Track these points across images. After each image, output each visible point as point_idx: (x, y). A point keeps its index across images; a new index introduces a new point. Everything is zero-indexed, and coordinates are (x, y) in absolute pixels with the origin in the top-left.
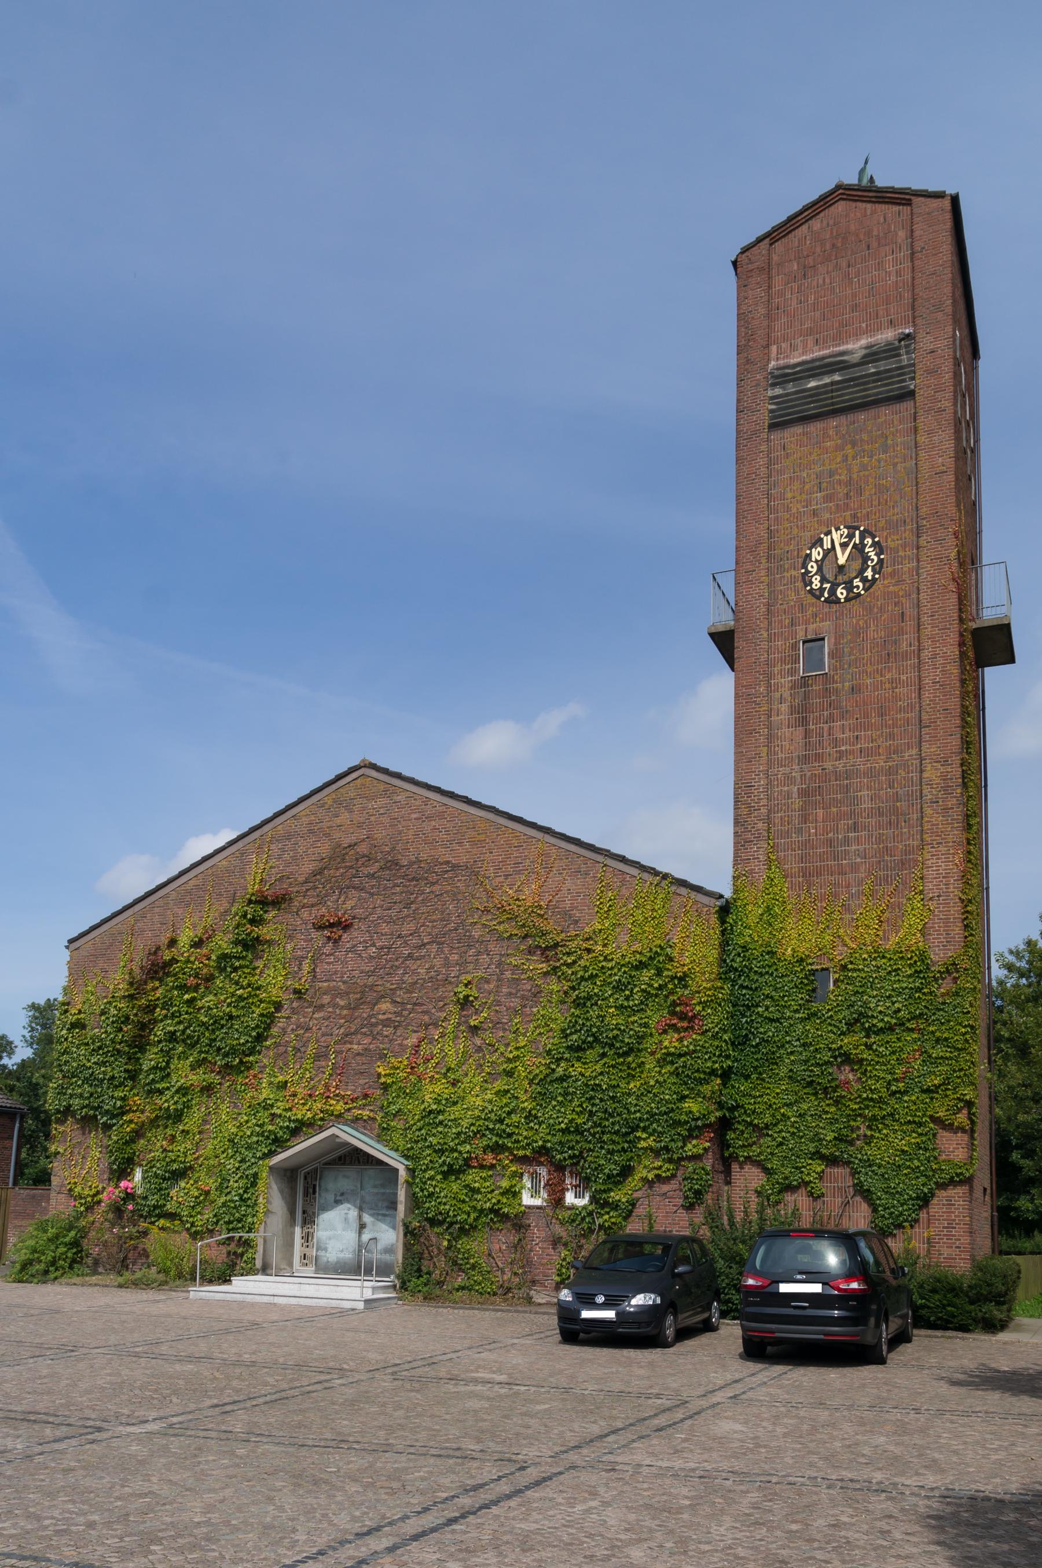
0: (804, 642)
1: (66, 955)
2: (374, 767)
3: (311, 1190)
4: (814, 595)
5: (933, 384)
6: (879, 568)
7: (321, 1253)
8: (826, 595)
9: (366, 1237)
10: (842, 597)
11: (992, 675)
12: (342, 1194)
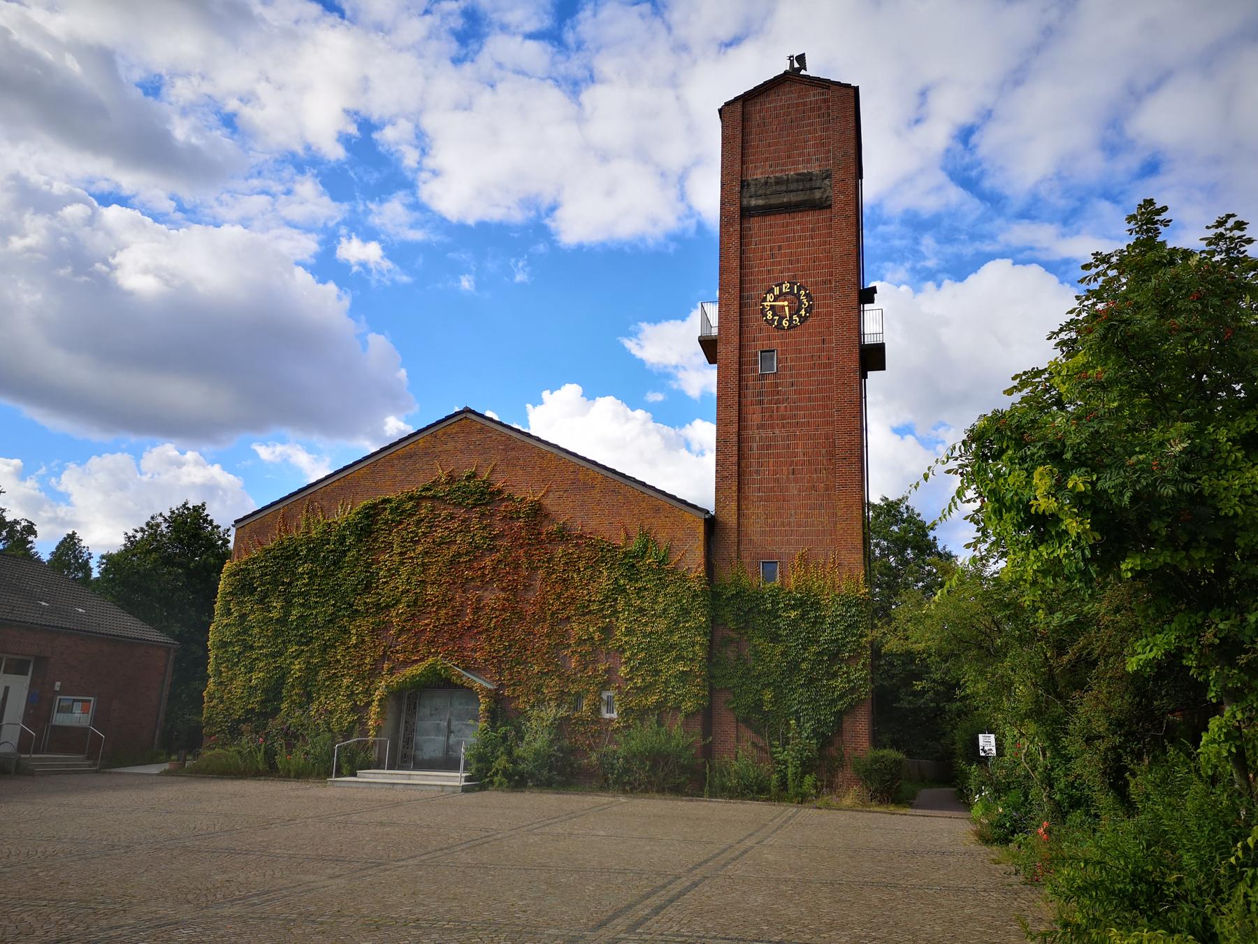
2: (473, 412)
7: (418, 753)
9: (453, 739)
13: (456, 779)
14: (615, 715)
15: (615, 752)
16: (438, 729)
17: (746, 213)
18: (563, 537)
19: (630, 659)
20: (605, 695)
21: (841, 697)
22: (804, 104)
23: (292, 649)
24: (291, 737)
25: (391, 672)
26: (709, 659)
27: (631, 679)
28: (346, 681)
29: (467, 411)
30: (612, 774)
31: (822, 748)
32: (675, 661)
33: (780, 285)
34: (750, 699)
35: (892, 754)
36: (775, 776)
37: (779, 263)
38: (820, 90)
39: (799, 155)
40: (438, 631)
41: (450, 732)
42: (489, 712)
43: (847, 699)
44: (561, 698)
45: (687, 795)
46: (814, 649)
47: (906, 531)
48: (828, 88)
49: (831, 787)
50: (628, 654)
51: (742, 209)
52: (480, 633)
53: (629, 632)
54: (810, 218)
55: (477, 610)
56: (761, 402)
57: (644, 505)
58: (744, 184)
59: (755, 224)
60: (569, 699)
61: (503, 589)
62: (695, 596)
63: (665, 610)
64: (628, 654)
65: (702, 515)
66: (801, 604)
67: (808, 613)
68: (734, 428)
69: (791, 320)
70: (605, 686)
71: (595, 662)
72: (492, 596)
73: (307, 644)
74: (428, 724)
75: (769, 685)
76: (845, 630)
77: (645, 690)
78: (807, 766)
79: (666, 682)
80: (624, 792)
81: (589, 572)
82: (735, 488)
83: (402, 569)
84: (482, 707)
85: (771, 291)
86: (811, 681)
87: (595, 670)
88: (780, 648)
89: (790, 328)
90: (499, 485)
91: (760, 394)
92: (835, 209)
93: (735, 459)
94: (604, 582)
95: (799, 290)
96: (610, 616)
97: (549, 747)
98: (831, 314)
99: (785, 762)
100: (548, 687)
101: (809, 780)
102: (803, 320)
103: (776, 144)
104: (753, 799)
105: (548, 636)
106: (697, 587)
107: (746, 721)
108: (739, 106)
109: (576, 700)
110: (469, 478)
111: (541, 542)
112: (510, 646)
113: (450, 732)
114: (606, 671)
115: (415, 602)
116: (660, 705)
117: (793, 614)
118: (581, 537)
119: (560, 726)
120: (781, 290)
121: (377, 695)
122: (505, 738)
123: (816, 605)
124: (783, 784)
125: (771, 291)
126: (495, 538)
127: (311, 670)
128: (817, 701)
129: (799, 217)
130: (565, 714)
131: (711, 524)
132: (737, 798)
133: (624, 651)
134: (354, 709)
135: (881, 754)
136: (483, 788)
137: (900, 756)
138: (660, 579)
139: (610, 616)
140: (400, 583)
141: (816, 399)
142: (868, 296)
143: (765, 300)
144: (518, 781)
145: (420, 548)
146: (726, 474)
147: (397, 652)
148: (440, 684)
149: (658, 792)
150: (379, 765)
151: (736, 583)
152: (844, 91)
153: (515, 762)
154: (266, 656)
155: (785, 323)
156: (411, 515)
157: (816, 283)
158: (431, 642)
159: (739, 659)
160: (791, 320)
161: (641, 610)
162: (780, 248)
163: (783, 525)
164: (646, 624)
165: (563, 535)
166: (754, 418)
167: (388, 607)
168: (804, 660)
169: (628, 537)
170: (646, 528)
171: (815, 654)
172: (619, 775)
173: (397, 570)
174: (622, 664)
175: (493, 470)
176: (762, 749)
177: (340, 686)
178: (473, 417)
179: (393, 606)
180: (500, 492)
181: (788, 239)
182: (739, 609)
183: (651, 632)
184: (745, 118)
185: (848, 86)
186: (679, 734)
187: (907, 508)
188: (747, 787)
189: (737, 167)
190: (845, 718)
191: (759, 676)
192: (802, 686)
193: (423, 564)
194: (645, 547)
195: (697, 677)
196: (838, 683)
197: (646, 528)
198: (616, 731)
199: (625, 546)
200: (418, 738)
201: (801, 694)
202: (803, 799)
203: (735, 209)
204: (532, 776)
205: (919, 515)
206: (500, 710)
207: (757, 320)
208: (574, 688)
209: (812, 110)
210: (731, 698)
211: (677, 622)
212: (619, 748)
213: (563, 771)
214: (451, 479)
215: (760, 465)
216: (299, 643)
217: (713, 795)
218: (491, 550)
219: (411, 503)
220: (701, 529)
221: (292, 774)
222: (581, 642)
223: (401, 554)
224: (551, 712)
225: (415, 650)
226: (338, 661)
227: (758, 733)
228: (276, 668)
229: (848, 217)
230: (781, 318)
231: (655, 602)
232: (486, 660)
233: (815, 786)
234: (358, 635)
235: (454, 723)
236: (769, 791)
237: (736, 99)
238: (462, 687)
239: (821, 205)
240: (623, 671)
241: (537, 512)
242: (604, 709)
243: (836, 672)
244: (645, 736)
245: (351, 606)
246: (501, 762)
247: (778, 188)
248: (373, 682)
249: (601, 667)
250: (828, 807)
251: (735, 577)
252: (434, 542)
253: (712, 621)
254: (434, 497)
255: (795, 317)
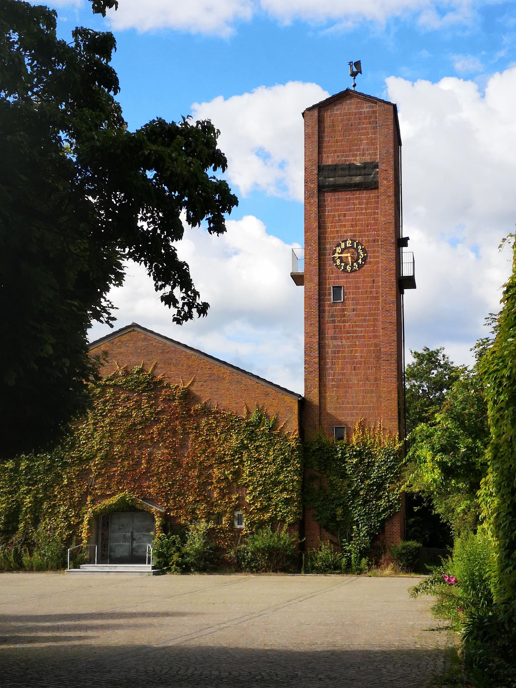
0: (333, 287)
1: (302, 120)
2: (139, 326)
3: (106, 524)
4: (337, 267)
5: (385, 183)
6: (364, 259)
7: (112, 554)
8: (342, 268)
9: (135, 544)
10: (349, 270)
11: (404, 249)
12: (122, 526)
13: (148, 568)
14: (243, 526)
15: (245, 549)
16: (125, 539)
17: (322, 189)
18: (205, 412)
19: (252, 491)
20: (236, 514)
21: (384, 511)
22: (361, 113)
23: (24, 488)
24: (30, 545)
25: (93, 502)
26: (302, 490)
27: (254, 504)
28: (62, 509)
29: (135, 326)
30: (244, 562)
31: (372, 542)
32: (281, 492)
33: (345, 241)
34: (328, 514)
35: (413, 544)
36: (344, 560)
37: (344, 226)
38: (370, 104)
39: (357, 150)
40: (123, 475)
41: (133, 539)
42: (445, 524)
43: (388, 512)
44: (208, 517)
45: (290, 572)
46: (368, 482)
47: (443, 375)
48: (376, 103)
49: (378, 565)
50: (251, 488)
51: (319, 186)
52: (153, 476)
53: (252, 474)
54: (365, 194)
55: (149, 461)
56: (334, 322)
57: (258, 391)
58: (321, 169)
59: (329, 197)
60: (213, 517)
61: (167, 448)
62: (293, 451)
63: (274, 460)
64: (251, 488)
65: (296, 398)
66: (359, 454)
67: (364, 459)
68: (316, 339)
69: (352, 266)
70: (237, 508)
71: (230, 493)
72: (161, 453)
73: (33, 485)
74: (117, 535)
75: (340, 505)
76: (387, 470)
77: (264, 509)
78: (363, 553)
79: (276, 505)
80: (252, 572)
81: (223, 436)
82: (317, 379)
83: (96, 435)
84: (158, 523)
85: (339, 245)
86: (366, 502)
87: (230, 498)
88: (347, 482)
89: (352, 271)
90: (160, 377)
91: (333, 316)
92: (381, 189)
93: (317, 360)
94: (234, 442)
95: (357, 246)
96: (237, 464)
97: (203, 547)
98: (378, 262)
99: (350, 551)
100: (199, 509)
101: (364, 561)
102: (360, 266)
103: (341, 141)
104: (331, 573)
105: (198, 477)
106: (293, 444)
107: (326, 528)
108: (316, 113)
109: (218, 518)
110: (138, 372)
111: (190, 416)
112: (173, 484)
113: (133, 539)
114: (237, 499)
115: (107, 455)
116: (272, 519)
117: (355, 461)
118: (217, 412)
119: (210, 534)
120: (345, 245)
121: (87, 517)
122: (174, 542)
123: (370, 455)
124: (349, 564)
125: (339, 245)
126: (159, 413)
127: (37, 502)
128: (370, 514)
129: (357, 194)
130: (212, 526)
131: (303, 403)
132: (322, 573)
133: (249, 486)
134: (70, 527)
135: (407, 544)
136: (163, 573)
137: (419, 545)
138: (271, 440)
139: (237, 464)
140: (95, 444)
141: (369, 321)
142: (403, 242)
143: (334, 252)
144: (185, 569)
145: (107, 421)
146: (311, 370)
147: (96, 489)
148: (126, 508)
149: (273, 571)
150: (91, 561)
151: (319, 441)
152: (386, 106)
153: (182, 556)
154: (5, 493)
155: (349, 268)
156: (99, 398)
157: (369, 241)
158: (119, 483)
159: (321, 489)
160: (352, 266)
161: (259, 460)
162: (345, 215)
163: (348, 403)
164: (262, 469)
165: (206, 411)
166: (329, 332)
167: (88, 459)
168: (361, 489)
169: (249, 413)
170: (260, 407)
171: (368, 485)
172: (249, 563)
173: (92, 434)
174: (247, 494)
175: (155, 367)
176: (335, 544)
177: (58, 512)
178: (139, 330)
179: (91, 459)
180: (161, 381)
181: (349, 210)
182: (320, 458)
183: (266, 474)
184: (320, 121)
185: (389, 103)
186: (285, 537)
187: (444, 356)
188: (327, 566)
189: (315, 155)
190: (386, 524)
191: (334, 500)
192: (360, 505)
193: (110, 431)
194: (260, 418)
195: (295, 501)
196: (382, 502)
197: (260, 407)
198: (246, 536)
199: (248, 418)
200: (112, 544)
201: (360, 510)
202: (360, 572)
203: (314, 186)
204: (193, 565)
205: (452, 363)
206: (169, 526)
207: (330, 265)
208: (217, 510)
209: (366, 118)
210: (316, 513)
211: (282, 468)
212: (248, 547)
213: (213, 561)
214: (127, 373)
215: (333, 364)
216: (28, 484)
217: (307, 572)
218: (157, 421)
219: (99, 390)
220: (296, 407)
221: (49, 567)
222: (219, 481)
223: (94, 424)
224: (203, 525)
225: (109, 487)
226: (56, 496)
227: (333, 533)
228: (13, 501)
229: (389, 196)
230: (346, 265)
231: (267, 454)
232: (157, 494)
233: (368, 565)
234: (69, 479)
235: (136, 534)
236: (341, 568)
237: (314, 107)
238: (143, 511)
239: (373, 186)
240: (248, 499)
241: (188, 397)
242: (236, 523)
243: (382, 496)
244: (264, 539)
245: (62, 459)
246: (175, 558)
247: (344, 173)
248: (80, 509)
249: (234, 497)
250: (375, 576)
251: (318, 437)
252: (117, 415)
253: (304, 466)
254: (115, 386)
255: (355, 264)
